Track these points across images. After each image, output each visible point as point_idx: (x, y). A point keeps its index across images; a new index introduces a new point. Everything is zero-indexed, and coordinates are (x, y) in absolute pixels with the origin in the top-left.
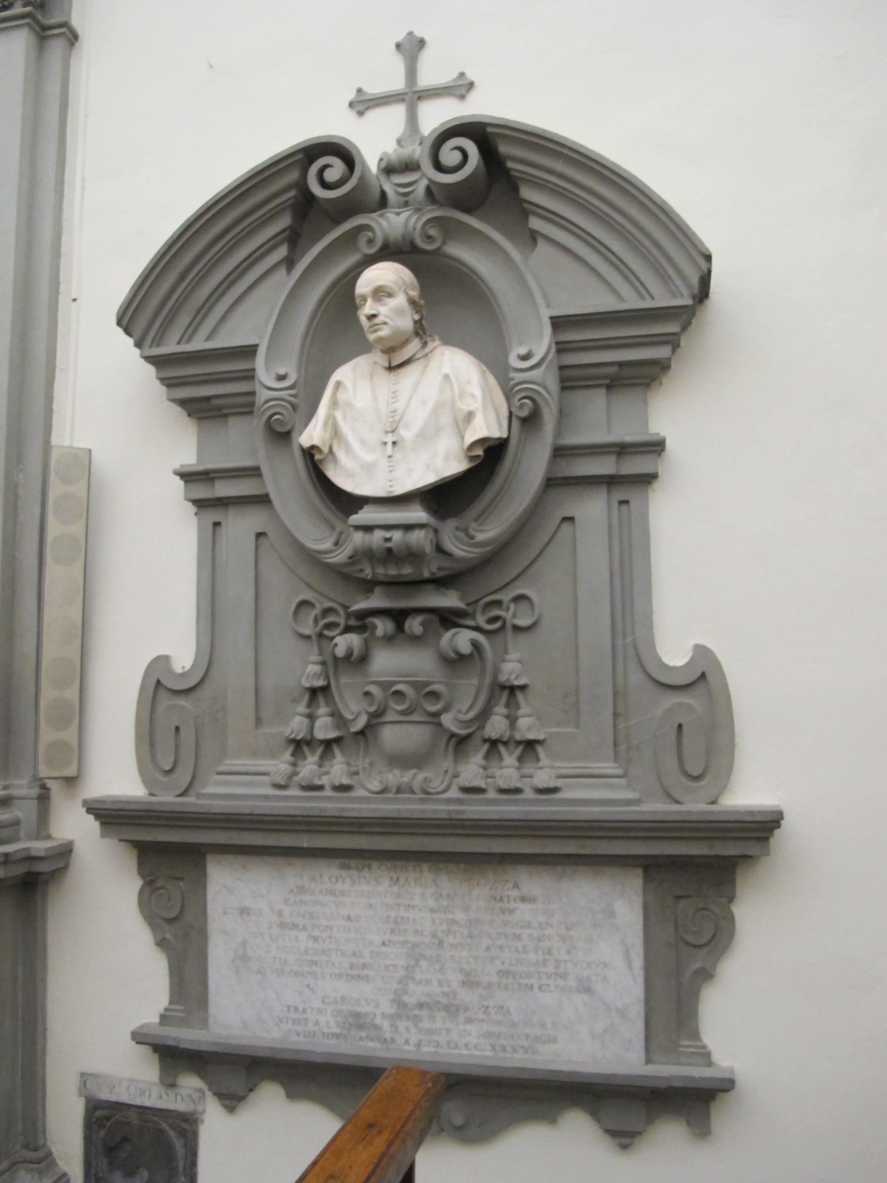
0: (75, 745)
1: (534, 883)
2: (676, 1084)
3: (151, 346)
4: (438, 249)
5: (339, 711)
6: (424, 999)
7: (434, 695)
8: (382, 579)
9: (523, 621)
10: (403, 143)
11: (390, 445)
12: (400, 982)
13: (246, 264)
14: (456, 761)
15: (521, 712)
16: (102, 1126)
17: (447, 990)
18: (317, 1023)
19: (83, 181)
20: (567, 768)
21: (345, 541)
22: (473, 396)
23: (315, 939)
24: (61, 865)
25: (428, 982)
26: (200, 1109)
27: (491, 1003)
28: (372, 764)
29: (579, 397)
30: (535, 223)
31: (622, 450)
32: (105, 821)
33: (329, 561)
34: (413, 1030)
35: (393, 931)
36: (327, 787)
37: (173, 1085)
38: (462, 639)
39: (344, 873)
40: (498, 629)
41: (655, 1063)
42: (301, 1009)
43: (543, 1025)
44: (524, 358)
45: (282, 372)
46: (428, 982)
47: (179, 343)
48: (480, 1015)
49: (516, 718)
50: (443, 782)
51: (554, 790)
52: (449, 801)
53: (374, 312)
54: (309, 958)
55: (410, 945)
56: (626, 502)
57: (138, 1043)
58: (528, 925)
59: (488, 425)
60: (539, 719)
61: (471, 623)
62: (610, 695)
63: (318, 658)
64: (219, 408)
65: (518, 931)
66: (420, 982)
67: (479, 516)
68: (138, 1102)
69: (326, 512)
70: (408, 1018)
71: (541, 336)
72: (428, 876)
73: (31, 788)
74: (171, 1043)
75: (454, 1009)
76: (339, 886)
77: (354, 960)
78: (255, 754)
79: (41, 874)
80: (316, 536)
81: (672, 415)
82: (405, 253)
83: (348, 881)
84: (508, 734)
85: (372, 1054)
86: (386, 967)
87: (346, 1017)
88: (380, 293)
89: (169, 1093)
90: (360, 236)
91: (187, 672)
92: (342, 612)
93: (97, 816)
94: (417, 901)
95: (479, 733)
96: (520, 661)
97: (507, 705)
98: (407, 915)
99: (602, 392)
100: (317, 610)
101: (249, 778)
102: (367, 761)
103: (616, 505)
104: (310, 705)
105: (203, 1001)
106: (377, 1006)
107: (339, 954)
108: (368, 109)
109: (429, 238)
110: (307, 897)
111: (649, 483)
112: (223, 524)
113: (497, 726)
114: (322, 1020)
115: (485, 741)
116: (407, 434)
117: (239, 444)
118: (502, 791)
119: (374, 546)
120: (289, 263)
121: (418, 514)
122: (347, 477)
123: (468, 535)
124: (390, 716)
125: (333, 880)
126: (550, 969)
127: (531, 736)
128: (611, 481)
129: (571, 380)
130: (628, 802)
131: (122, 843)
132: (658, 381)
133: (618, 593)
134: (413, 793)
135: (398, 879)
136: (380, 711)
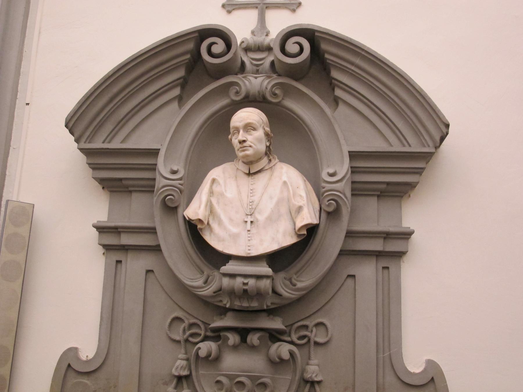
3: (85, 142)
4: (280, 102)
8: (236, 308)
9: (321, 339)
10: (256, 34)
11: (249, 223)
13: (154, 95)
19: (40, 28)
21: (212, 281)
22: (301, 196)
29: (361, 200)
30: (338, 92)
31: (387, 236)
33: (198, 293)
38: (283, 349)
40: (306, 344)
44: (332, 175)
45: (175, 168)
47: (103, 142)
53: (244, 139)
59: (308, 217)
61: (288, 339)
63: (184, 356)
64: (127, 187)
67: (298, 272)
69: (198, 261)
71: (342, 163)
80: (192, 278)
81: (413, 216)
82: (260, 102)
88: (249, 127)
90: (231, 88)
91: (91, 360)
92: (202, 326)
96: (318, 365)
99: (376, 198)
103: (381, 268)
108: (234, 9)
109: (275, 94)
111: (401, 257)
116: (261, 217)
117: (137, 211)
120: (180, 99)
121: (265, 269)
122: (219, 240)
123: (291, 283)
128: (378, 255)
129: (358, 191)
132: (407, 195)
133: (381, 324)
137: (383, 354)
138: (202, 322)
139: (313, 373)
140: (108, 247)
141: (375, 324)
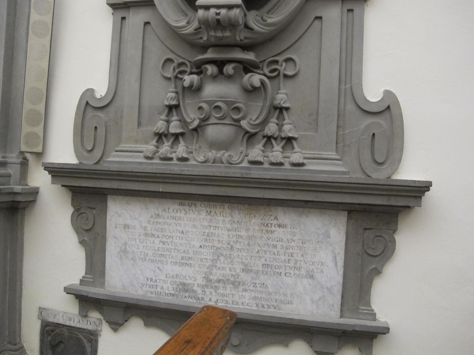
0: (41, 135)
1: (285, 217)
2: (357, 329)
5: (184, 119)
6: (221, 278)
7: (238, 109)
12: (208, 268)
14: (247, 148)
15: (286, 121)
16: (49, 335)
17: (233, 273)
18: (162, 288)
19: (336, 265)
20: (309, 154)
23: (164, 243)
24: (31, 199)
25: (224, 269)
26: (99, 329)
27: (258, 282)
28: (200, 147)
32: (53, 174)
33: (183, 32)
34: (214, 293)
35: (206, 240)
36: (175, 159)
37: (86, 316)
38: (255, 79)
39: (181, 208)
40: (275, 76)
41: (345, 318)
42: (154, 280)
43: (285, 295)
46: (224, 269)
48: (251, 288)
49: (283, 125)
50: (239, 158)
51: (302, 165)
52: (242, 168)
54: (160, 253)
55: (215, 248)
56: (352, 10)
57: (67, 293)
58: (282, 240)
60: (295, 127)
62: (336, 116)
63: (174, 90)
65: (275, 243)
66: (219, 268)
68: (68, 324)
70: (212, 287)
72: (227, 210)
73: (17, 159)
74: (84, 294)
75: (237, 284)
76: (178, 215)
77: (184, 255)
78: (136, 142)
79: (19, 202)
83: (183, 212)
84: (277, 133)
85: (190, 305)
86: (201, 260)
87: (178, 285)
89: (84, 320)
93: (50, 172)
94: (221, 225)
95: (261, 133)
96: (286, 94)
97: (278, 118)
98: (214, 231)
100: (175, 64)
101: (132, 152)
102: (197, 146)
103: (346, 11)
104: (167, 116)
105: (102, 273)
106: (195, 280)
107: (176, 251)
110: (161, 220)
112: (126, 18)
113: (271, 128)
114: (165, 286)
115: (264, 137)
118: (272, 164)
119: (210, 18)
124: (212, 120)
125: (175, 211)
126: (292, 264)
127: (290, 135)
130: (344, 173)
131: (63, 188)
133: (344, 60)
134: (223, 163)
135: (211, 212)
136: (206, 118)
137: (345, 86)
138: (189, 61)
139: (281, 100)
140: (115, 7)
141: (339, 59)
